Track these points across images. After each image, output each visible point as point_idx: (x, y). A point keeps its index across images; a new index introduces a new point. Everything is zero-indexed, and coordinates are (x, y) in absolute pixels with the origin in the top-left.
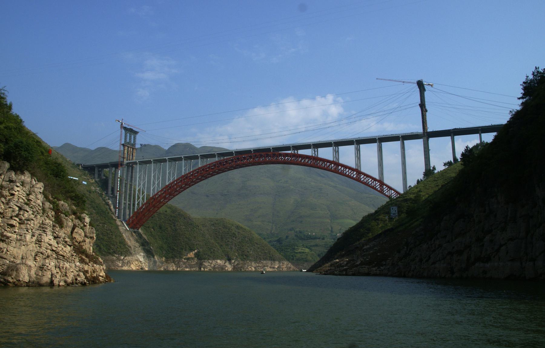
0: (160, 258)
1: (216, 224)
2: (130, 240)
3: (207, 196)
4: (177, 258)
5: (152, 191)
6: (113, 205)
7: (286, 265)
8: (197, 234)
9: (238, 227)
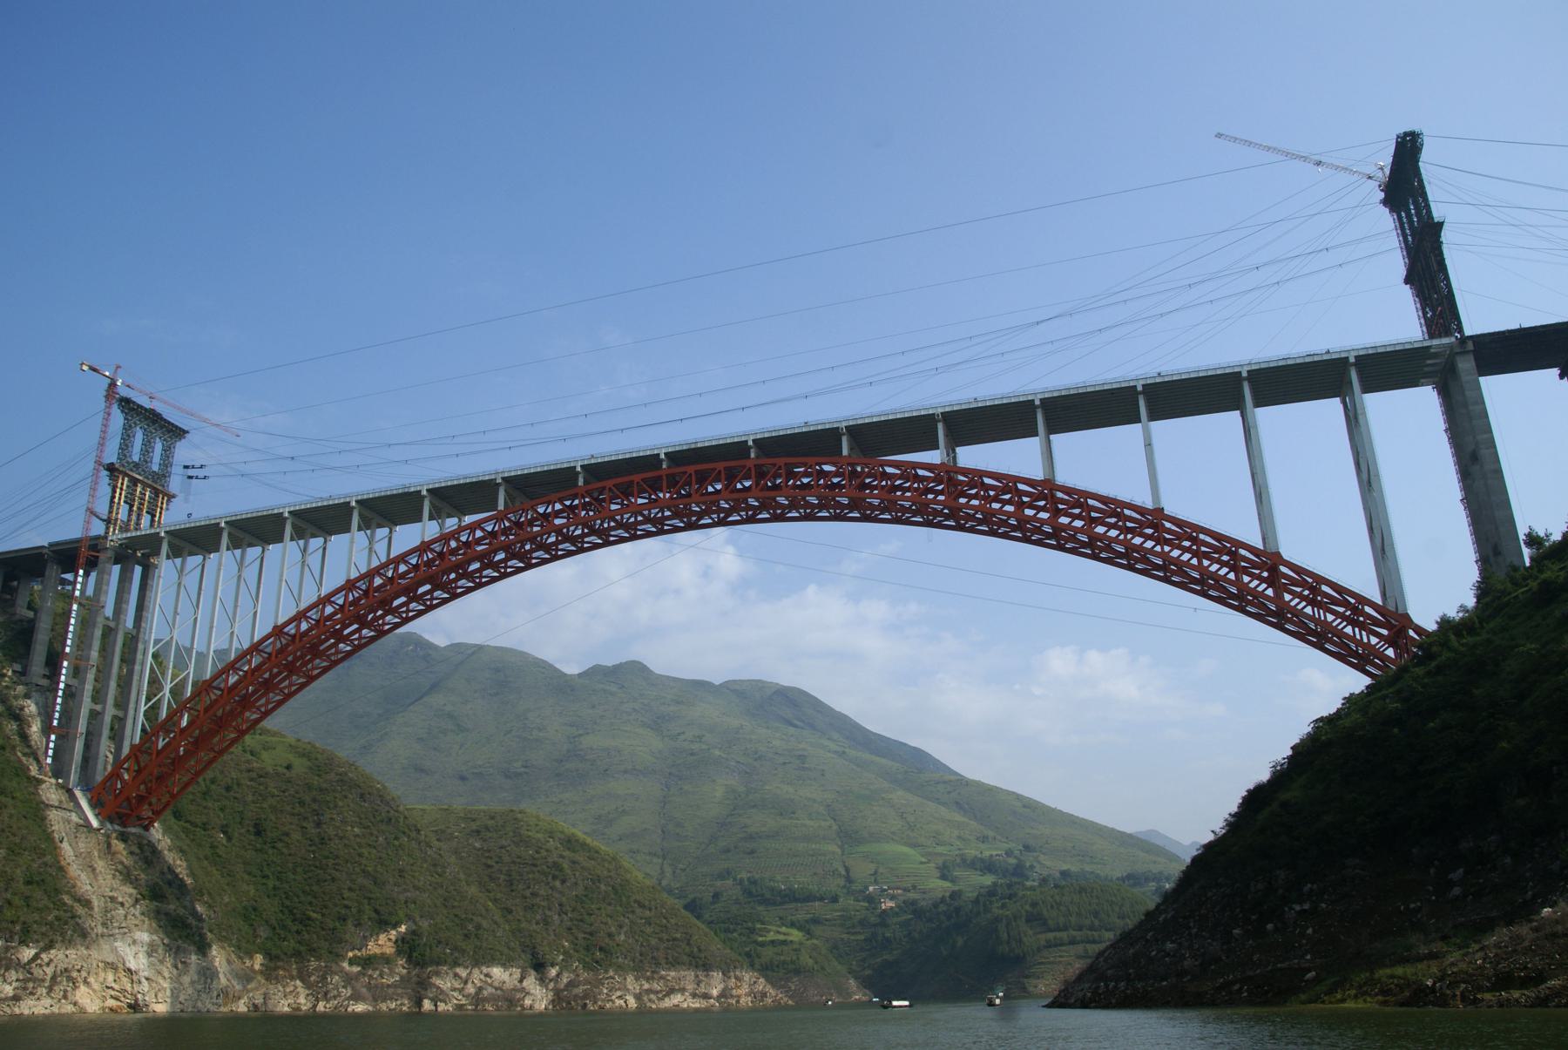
0: (240, 958)
1: (487, 829)
2: (94, 870)
3: (463, 778)
4: (319, 959)
6: (42, 721)
7: (750, 985)
8: (412, 861)
9: (570, 842)
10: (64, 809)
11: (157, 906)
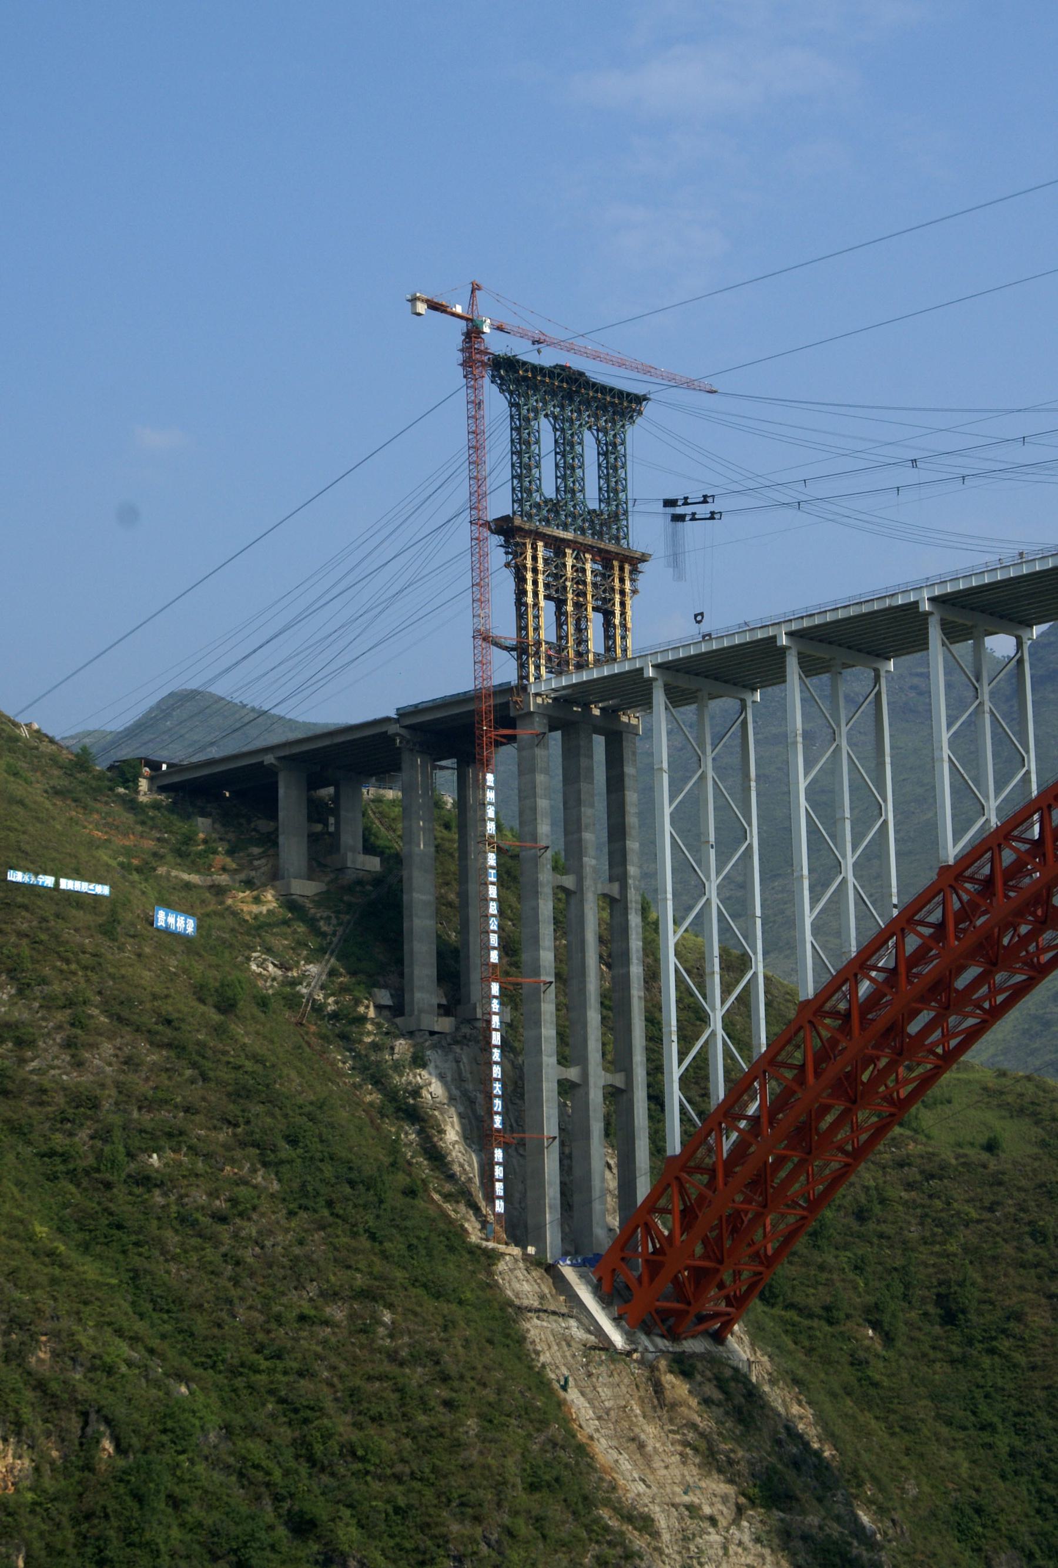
2: (642, 1446)
5: (809, 937)
6: (461, 1116)
10: (554, 1313)
11: (782, 1520)
